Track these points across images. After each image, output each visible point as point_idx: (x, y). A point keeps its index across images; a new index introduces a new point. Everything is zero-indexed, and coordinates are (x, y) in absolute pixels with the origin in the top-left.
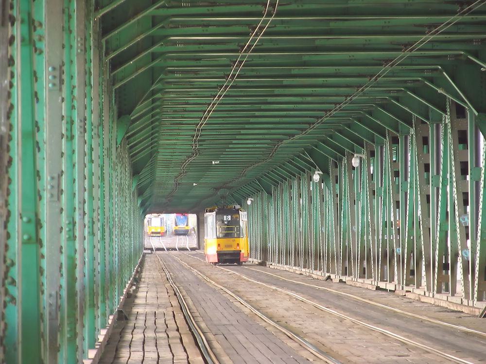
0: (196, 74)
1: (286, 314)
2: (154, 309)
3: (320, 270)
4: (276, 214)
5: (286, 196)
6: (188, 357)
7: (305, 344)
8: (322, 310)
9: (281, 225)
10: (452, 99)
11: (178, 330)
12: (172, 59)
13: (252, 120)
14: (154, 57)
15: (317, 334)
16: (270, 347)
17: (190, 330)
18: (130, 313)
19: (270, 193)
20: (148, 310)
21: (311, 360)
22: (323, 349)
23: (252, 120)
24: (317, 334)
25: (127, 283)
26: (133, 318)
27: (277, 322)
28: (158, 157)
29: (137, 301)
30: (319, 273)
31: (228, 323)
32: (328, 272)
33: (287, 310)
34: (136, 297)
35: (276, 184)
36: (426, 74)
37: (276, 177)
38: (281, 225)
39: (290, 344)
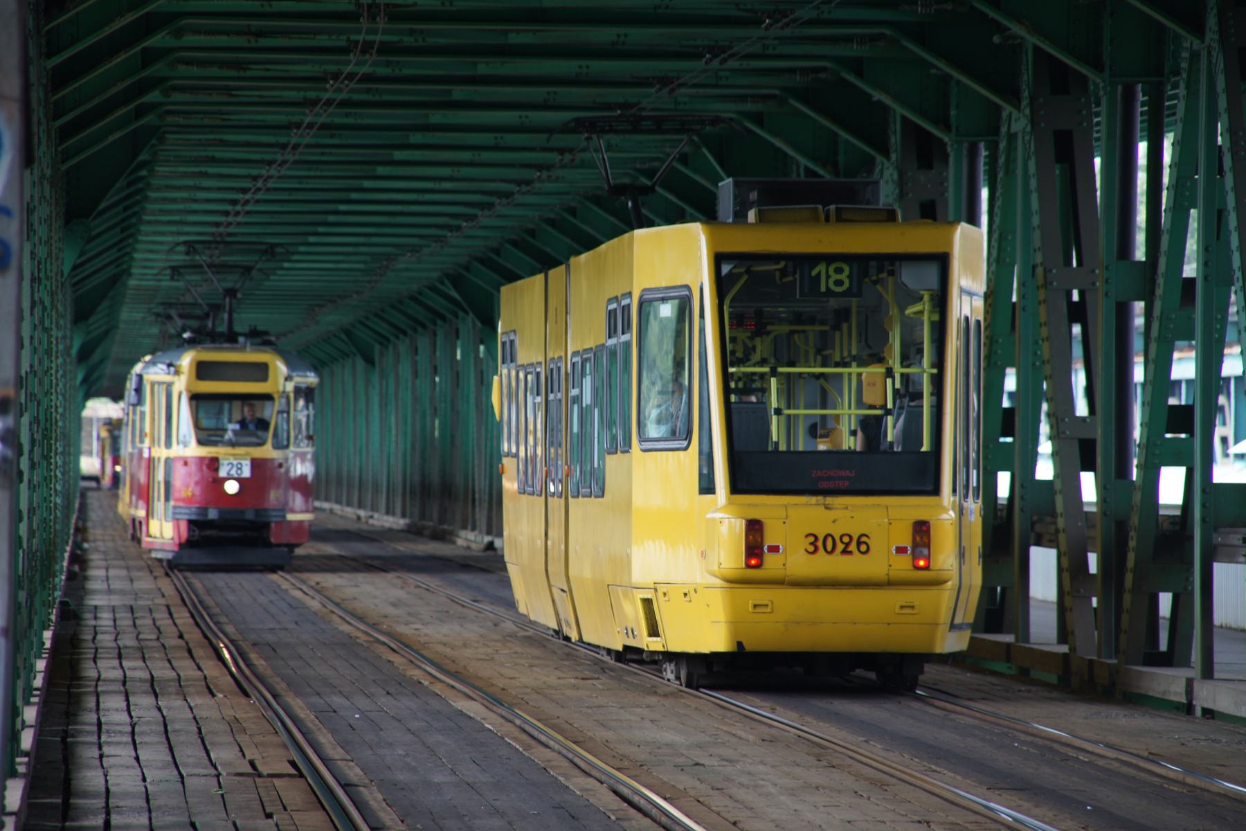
0: (231, 95)
1: (391, 611)
2: (129, 601)
3: (473, 529)
4: (383, 406)
5: (405, 369)
6: (199, 729)
7: (403, 650)
8: (463, 606)
9: (393, 432)
10: (811, 165)
11: (181, 636)
12: (189, 62)
13: (331, 218)
14: (149, 57)
15: (445, 645)
16: (355, 665)
17: (206, 637)
18: (80, 604)
19: (370, 361)
20: (116, 600)
21: (426, 683)
22: (452, 668)
23: (331, 218)
24: (445, 645)
25: (66, 551)
26: (88, 616)
27: (374, 626)
28: (143, 228)
29: (91, 585)
30: (471, 536)
31: (278, 626)
32: (489, 533)
33: (394, 605)
34: (86, 578)
35: (384, 341)
36: (854, 50)
37: (383, 328)
38: (393, 432)
39: (396, 659)
